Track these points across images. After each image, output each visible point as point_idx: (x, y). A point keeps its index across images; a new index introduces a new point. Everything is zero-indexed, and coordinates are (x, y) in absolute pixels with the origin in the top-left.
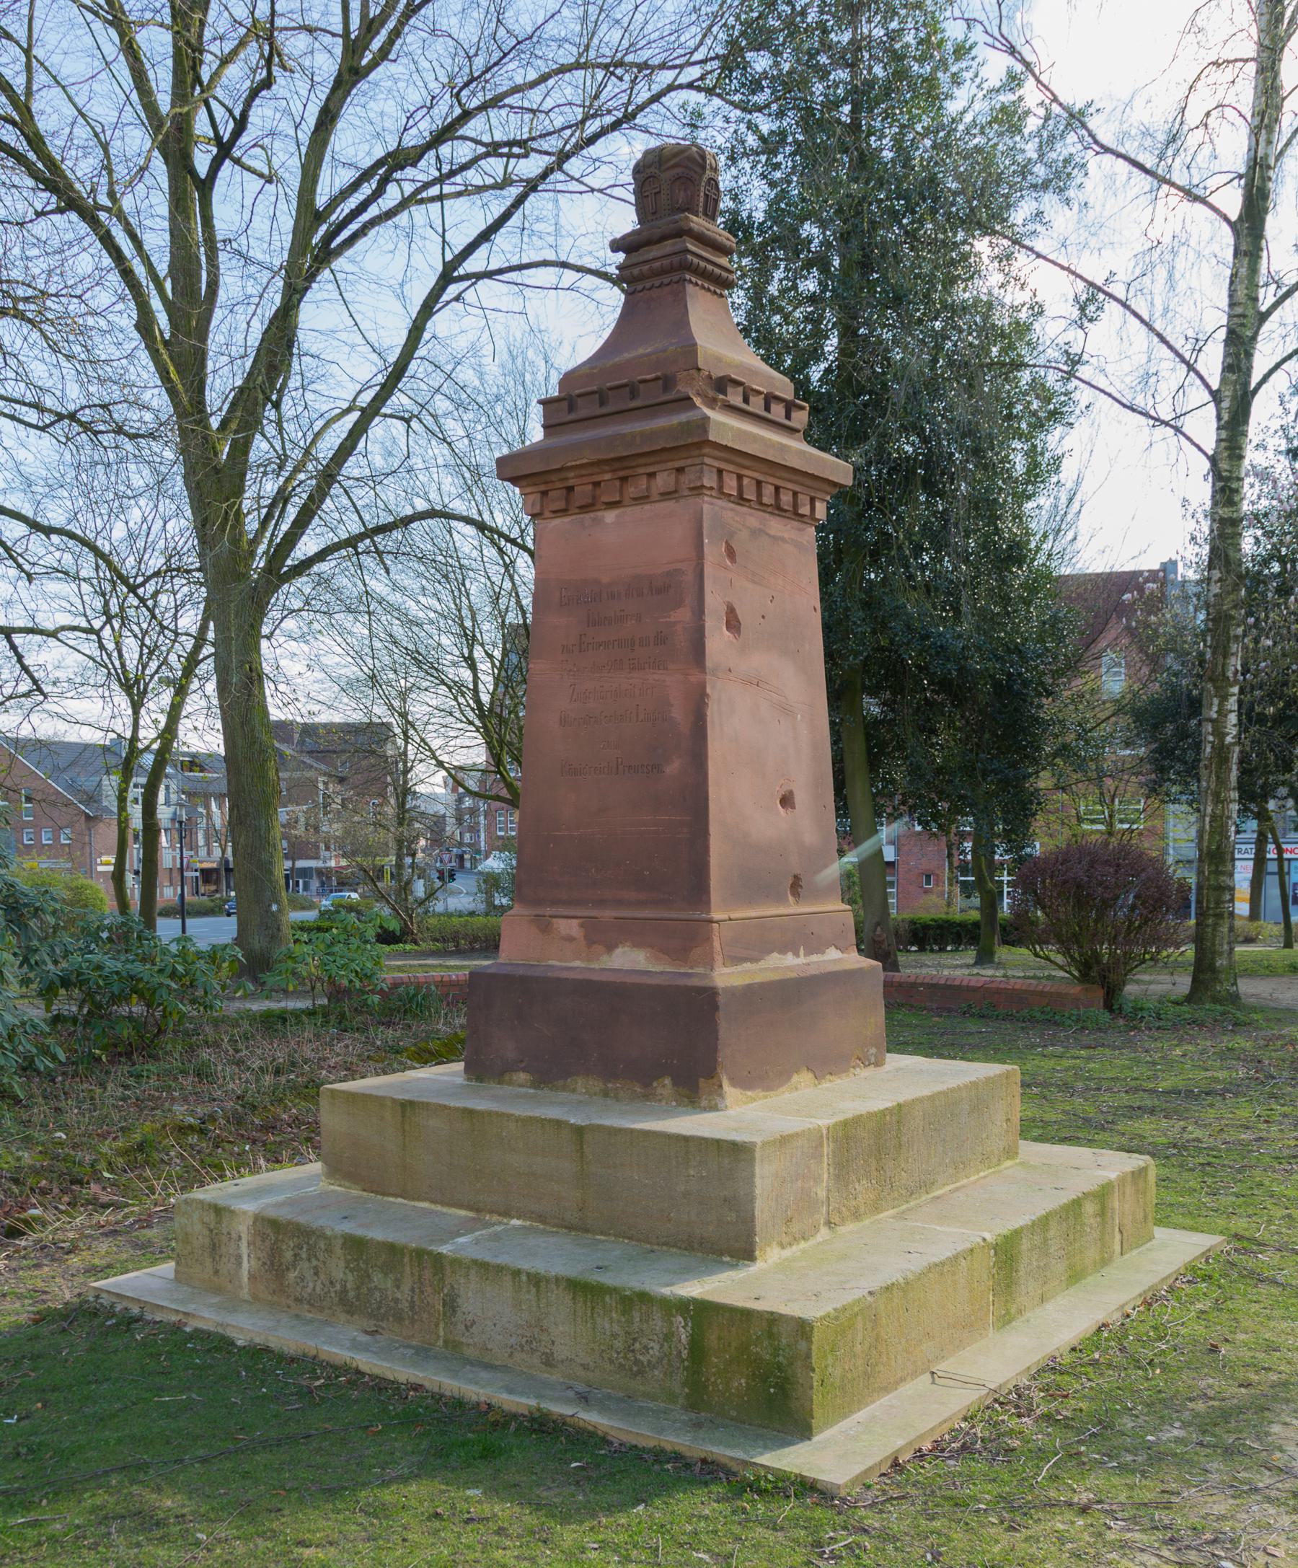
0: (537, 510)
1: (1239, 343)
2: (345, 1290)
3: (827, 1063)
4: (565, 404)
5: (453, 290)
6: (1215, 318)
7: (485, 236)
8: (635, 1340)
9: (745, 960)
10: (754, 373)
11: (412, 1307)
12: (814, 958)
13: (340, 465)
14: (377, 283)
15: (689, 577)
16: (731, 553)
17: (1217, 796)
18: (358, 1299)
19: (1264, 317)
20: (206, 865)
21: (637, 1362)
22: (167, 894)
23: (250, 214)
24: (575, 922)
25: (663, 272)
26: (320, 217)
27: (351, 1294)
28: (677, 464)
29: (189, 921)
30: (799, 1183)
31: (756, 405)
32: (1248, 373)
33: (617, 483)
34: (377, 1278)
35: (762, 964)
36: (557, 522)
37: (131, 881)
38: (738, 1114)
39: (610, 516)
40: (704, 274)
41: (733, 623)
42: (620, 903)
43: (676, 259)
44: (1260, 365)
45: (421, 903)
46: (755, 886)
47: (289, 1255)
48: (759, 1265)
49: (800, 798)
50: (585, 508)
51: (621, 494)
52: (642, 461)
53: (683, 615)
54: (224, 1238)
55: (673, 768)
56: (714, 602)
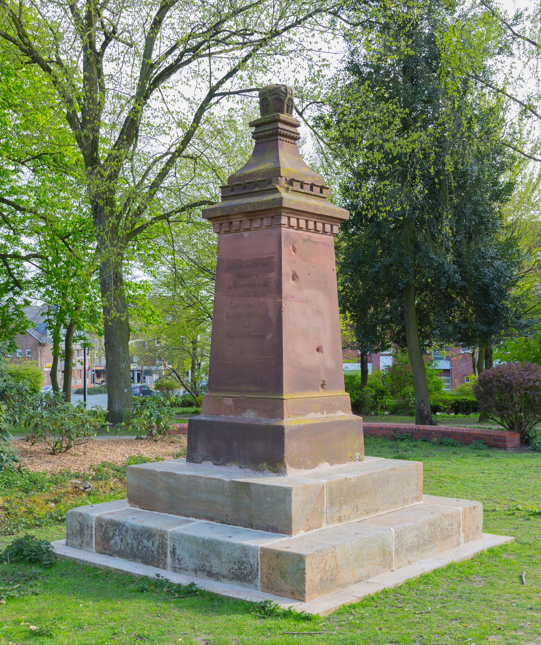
0: (218, 231)
2: (132, 548)
4: (229, 189)
5: (214, 100)
7: (230, 75)
8: (241, 565)
9: (299, 415)
11: (158, 552)
12: (331, 415)
13: (162, 180)
14: (182, 92)
15: (276, 260)
16: (294, 250)
18: (137, 550)
20: (98, 368)
21: (242, 573)
22: (77, 382)
23: (121, 70)
24: (231, 399)
25: (266, 136)
26: (152, 66)
27: (135, 549)
28: (271, 215)
29: (88, 397)
30: (313, 505)
31: (307, 189)
33: (249, 221)
34: (145, 541)
35: (306, 417)
36: (226, 235)
37: (60, 376)
39: (246, 234)
40: (286, 136)
41: (295, 277)
42: (249, 391)
43: (274, 131)
45: (51, 404)
46: (304, 384)
47: (111, 534)
48: (294, 537)
49: (326, 348)
50: (236, 231)
51: (251, 225)
52: (258, 213)
53: (273, 275)
54: (86, 527)
55: (269, 337)
56: (286, 269)
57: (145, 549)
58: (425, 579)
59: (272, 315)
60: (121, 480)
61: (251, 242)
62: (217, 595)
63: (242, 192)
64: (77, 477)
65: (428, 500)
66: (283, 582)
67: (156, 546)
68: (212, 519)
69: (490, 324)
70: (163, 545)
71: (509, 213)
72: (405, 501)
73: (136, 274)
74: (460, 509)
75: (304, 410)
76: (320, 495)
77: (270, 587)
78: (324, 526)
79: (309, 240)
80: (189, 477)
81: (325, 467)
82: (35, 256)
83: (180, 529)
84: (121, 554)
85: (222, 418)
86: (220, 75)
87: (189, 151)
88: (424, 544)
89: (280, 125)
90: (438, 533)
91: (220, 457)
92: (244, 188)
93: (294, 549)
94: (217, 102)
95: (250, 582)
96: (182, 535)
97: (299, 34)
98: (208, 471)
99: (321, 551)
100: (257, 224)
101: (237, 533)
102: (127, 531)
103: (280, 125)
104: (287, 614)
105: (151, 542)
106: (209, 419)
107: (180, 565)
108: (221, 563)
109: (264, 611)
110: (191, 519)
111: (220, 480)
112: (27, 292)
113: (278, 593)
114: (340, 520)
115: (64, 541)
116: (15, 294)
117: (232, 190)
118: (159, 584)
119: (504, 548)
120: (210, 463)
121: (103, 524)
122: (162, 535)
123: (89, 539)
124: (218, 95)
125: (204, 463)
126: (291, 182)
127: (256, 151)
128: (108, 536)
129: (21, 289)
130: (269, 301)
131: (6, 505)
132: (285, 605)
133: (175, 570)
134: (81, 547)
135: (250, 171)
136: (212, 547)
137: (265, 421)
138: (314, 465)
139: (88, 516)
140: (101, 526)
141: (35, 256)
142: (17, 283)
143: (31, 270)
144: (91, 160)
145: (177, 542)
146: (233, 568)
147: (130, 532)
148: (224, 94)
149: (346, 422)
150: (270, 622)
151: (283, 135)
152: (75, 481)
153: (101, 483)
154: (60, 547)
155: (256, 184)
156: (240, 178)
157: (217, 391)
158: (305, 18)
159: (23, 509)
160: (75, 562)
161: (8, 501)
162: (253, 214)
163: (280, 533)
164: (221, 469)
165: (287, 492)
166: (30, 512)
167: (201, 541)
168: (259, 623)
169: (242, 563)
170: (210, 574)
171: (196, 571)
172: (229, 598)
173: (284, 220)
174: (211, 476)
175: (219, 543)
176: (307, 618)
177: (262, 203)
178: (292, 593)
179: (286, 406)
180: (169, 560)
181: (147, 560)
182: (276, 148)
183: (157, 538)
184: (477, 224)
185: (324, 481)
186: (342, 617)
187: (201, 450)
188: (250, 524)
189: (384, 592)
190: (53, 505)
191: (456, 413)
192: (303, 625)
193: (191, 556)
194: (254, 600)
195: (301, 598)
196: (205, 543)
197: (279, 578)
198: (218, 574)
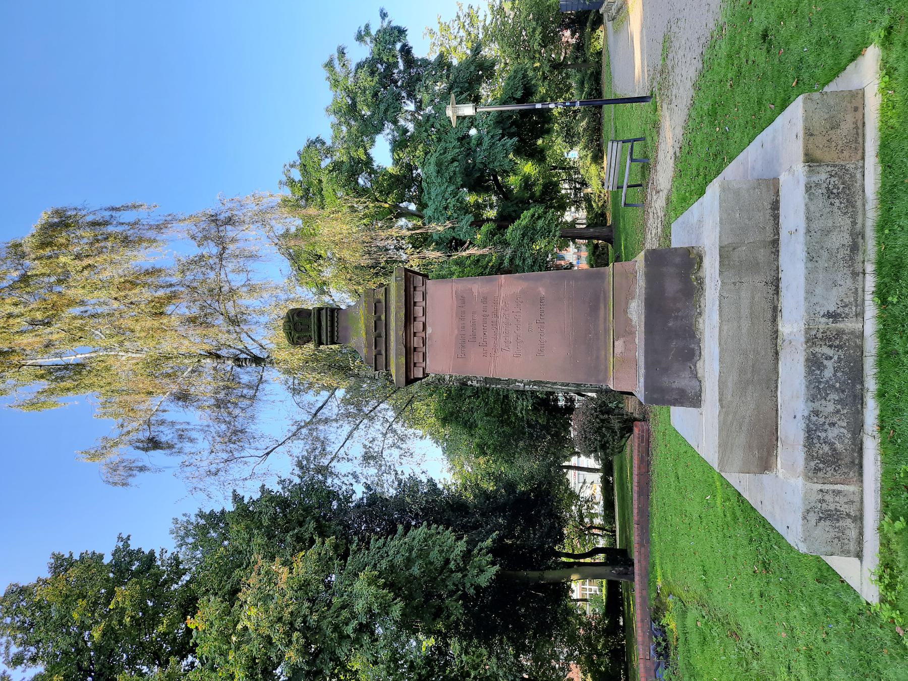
2: (840, 401)
8: (832, 193)
11: (839, 347)
28: (412, 289)
34: (828, 373)
39: (429, 330)
50: (424, 344)
57: (839, 374)
63: (384, 339)
67: (830, 352)
84: (857, 428)
85: (640, 356)
98: (710, 366)
105: (825, 362)
106: (642, 380)
107: (851, 303)
108: (835, 227)
113: (860, 131)
120: (699, 364)
121: (813, 464)
123: (842, 500)
133: (860, 315)
136: (816, 236)
140: (817, 470)
145: (818, 309)
146: (839, 208)
147: (817, 405)
163: (778, 195)
167: (810, 265)
169: (829, 192)
177: (398, 296)
178: (856, 109)
187: (682, 381)
195: (860, 96)
197: (839, 131)
198: (851, 235)
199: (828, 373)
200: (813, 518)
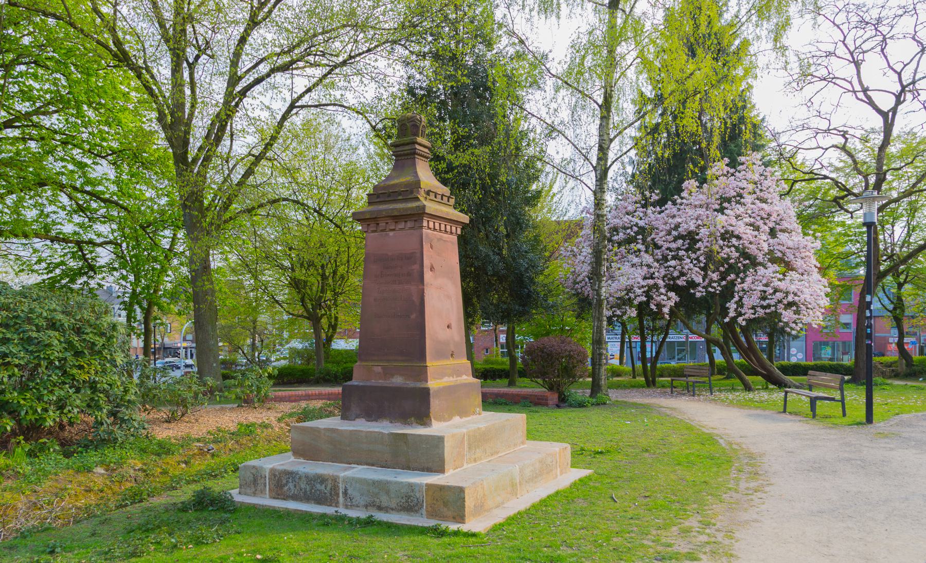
1: (603, 150)
2: (306, 492)
3: (463, 413)
5: (295, 111)
6: (594, 140)
7: (309, 90)
10: (437, 188)
11: (331, 494)
15: (418, 255)
17: (598, 318)
19: (611, 141)
25: (407, 154)
32: (606, 160)
34: (318, 486)
38: (436, 428)
39: (391, 234)
41: (432, 269)
42: (396, 361)
44: (611, 156)
46: (440, 355)
47: (284, 481)
48: (446, 474)
49: (454, 325)
50: (382, 231)
53: (416, 267)
55: (413, 316)
56: (426, 262)
58: (543, 502)
59: (415, 298)
60: (237, 442)
61: (396, 239)
62: (392, 523)
64: (198, 440)
65: (530, 445)
66: (445, 509)
67: (328, 488)
68: (373, 465)
69: (524, 306)
70: (335, 488)
71: (539, 214)
72: (515, 445)
73: (216, 262)
74: (557, 449)
75: (441, 375)
76: (462, 441)
77: (432, 514)
78: (465, 466)
79: (440, 239)
80: (351, 431)
81: (457, 419)
82: (110, 242)
83: (349, 473)
84: (295, 498)
86: (300, 89)
87: (270, 154)
88: (536, 477)
89: (417, 147)
90: (544, 470)
91: (372, 415)
92: (389, 196)
93: (453, 483)
94: (296, 113)
95: (417, 511)
96: (353, 478)
97: (369, 58)
98: (362, 426)
99: (474, 483)
100: (401, 225)
101: (399, 474)
102: (300, 478)
103: (417, 147)
104: (456, 533)
109: (439, 533)
110: (353, 465)
111: (380, 433)
112: (100, 276)
114: (475, 461)
115: (237, 490)
116: (89, 277)
117: (378, 197)
118: (340, 519)
119: (589, 478)
120: (363, 420)
122: (335, 480)
123: (262, 487)
124: (298, 107)
125: (357, 420)
126: (428, 193)
127: (396, 167)
128: (281, 483)
129: (95, 273)
130: (413, 288)
131: (144, 467)
132: (453, 527)
133: (346, 507)
134: (254, 494)
135: (392, 182)
136: (382, 486)
137: (411, 384)
138: (450, 419)
139: (262, 468)
140: (275, 476)
141: (110, 242)
142: (92, 268)
143: (104, 256)
144: (181, 158)
147: (304, 479)
148: (302, 107)
149: (470, 384)
150: (446, 540)
151: (419, 155)
152: (198, 444)
153: (222, 445)
154: (237, 497)
155: (400, 193)
156: (384, 188)
157: (366, 361)
158: (376, 46)
159: (159, 470)
160: (254, 506)
161: (145, 464)
162: (398, 218)
164: (374, 424)
165: (440, 439)
166: (165, 473)
168: (436, 541)
169: (409, 497)
170: (380, 508)
171: (366, 506)
172: (402, 525)
173: (425, 224)
174: (371, 430)
175: (388, 482)
176: (474, 535)
178: (454, 518)
179: (430, 371)
180: (341, 499)
181: (320, 501)
182: (414, 165)
183: (330, 482)
184: (517, 224)
185: (465, 430)
186: (497, 533)
188: (408, 467)
189: (519, 513)
190: (184, 465)
191: (485, 380)
192: (471, 540)
193: (362, 495)
194: (426, 525)
196: (374, 483)
198: (387, 507)
199: (318, 486)
200: (253, 471)
